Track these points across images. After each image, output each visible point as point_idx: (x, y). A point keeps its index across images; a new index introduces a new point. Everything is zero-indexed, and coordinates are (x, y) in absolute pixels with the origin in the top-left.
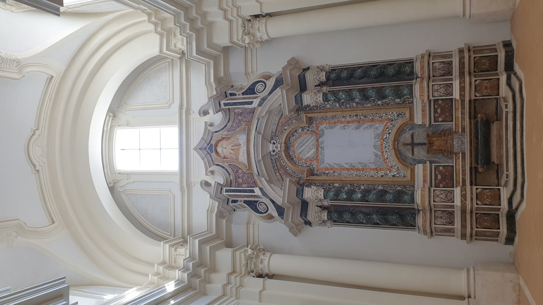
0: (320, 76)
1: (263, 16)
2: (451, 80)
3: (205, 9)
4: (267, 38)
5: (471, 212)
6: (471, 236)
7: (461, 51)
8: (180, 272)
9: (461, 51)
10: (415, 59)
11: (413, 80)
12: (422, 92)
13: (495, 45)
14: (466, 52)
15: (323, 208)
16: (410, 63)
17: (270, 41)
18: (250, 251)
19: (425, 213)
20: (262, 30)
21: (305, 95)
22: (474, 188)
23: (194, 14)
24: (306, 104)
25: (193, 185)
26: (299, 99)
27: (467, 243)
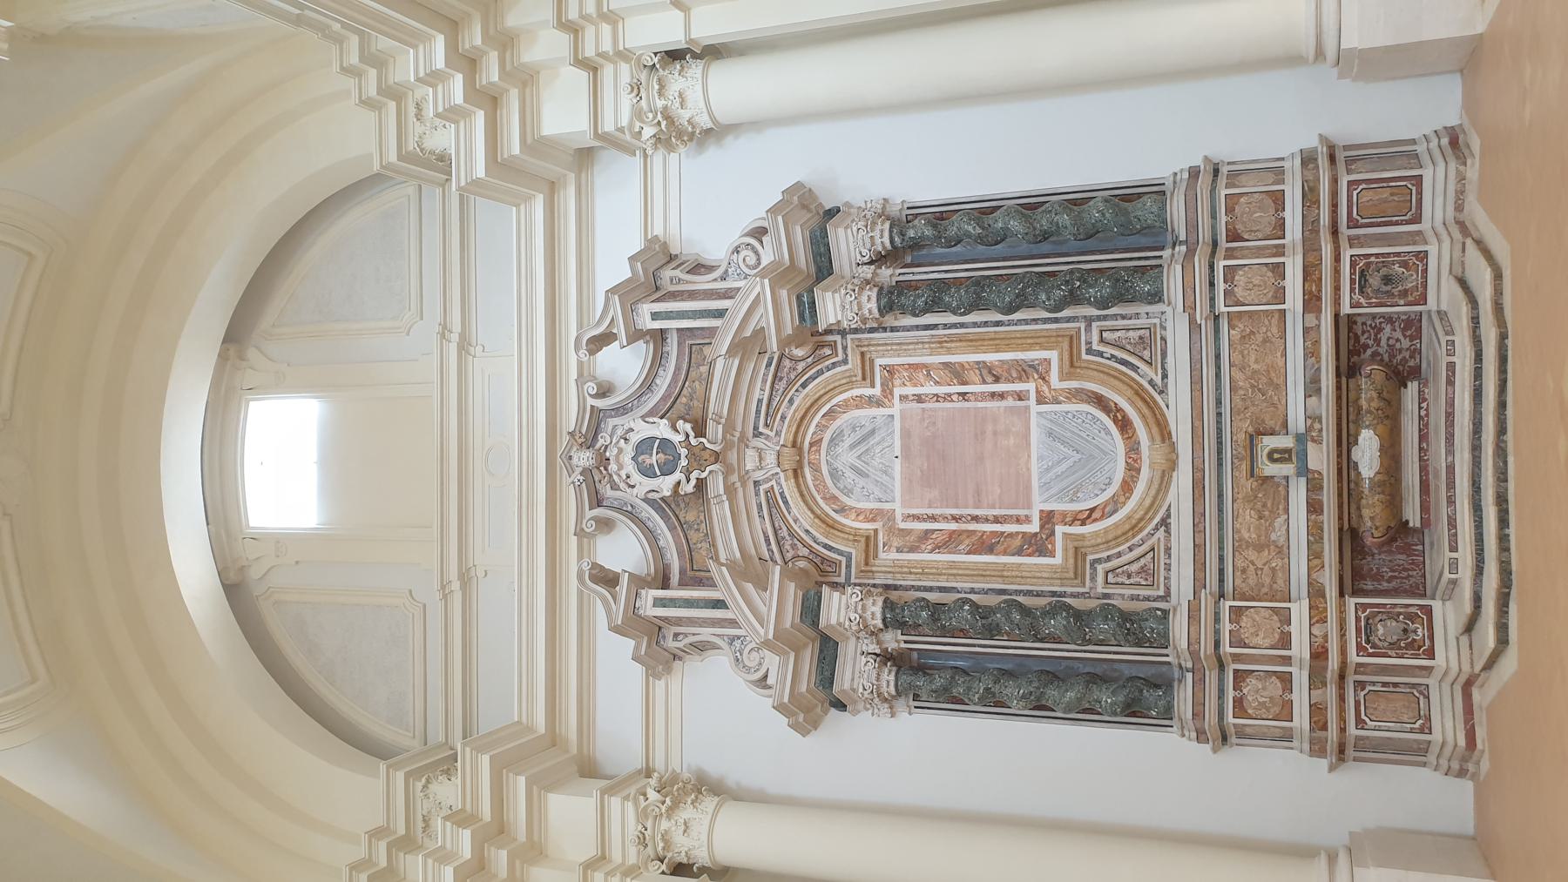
0: (877, 234)
1: (695, 56)
2: (1280, 251)
3: (512, 20)
4: (710, 125)
5: (1342, 677)
6: (1341, 750)
7: (1308, 159)
8: (430, 861)
9: (1308, 159)
10: (1169, 183)
11: (1162, 248)
12: (1188, 288)
13: (1413, 142)
14: (1323, 162)
15: (885, 657)
16: (1157, 192)
17: (714, 134)
18: (653, 795)
19: (1198, 671)
20: (695, 94)
21: (841, 231)
22: (1351, 602)
23: (478, 41)
24: (832, 320)
25: (481, 574)
26: (807, 309)
27: (1332, 768)
